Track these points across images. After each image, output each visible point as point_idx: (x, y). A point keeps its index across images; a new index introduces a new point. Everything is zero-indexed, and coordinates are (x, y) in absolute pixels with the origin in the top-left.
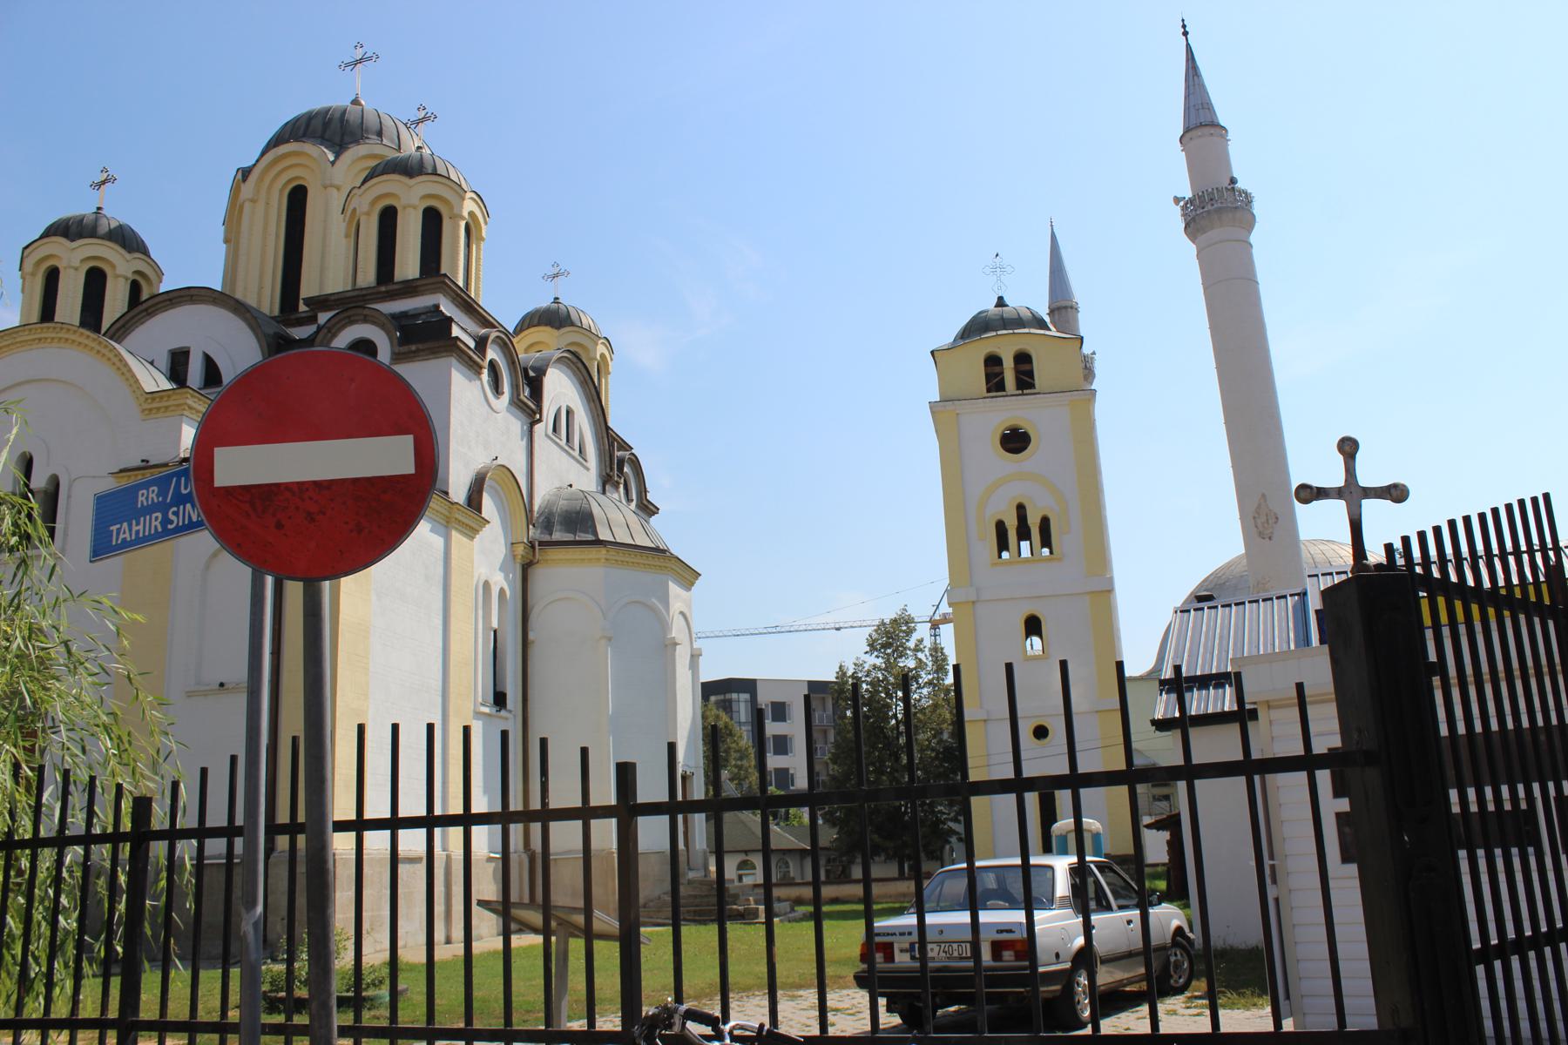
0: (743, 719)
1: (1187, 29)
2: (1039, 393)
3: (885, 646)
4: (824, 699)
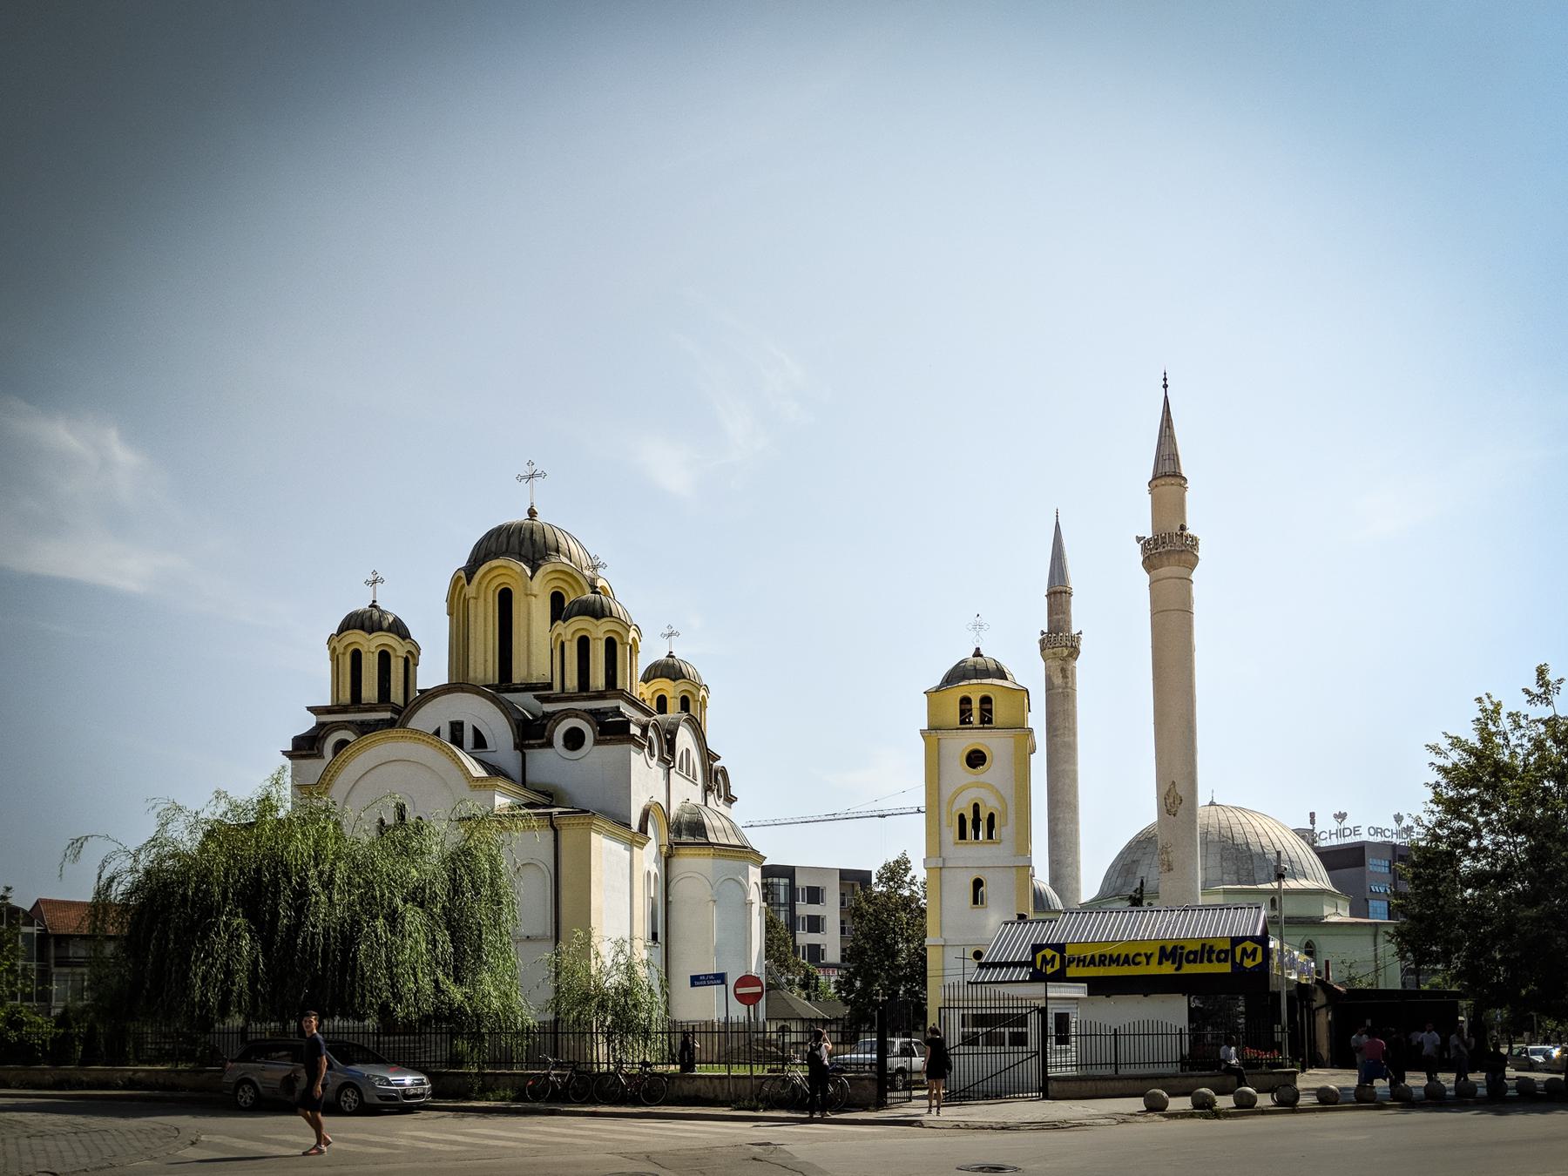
0: (782, 901)
1: (1163, 383)
2: (994, 728)
3: (889, 879)
4: (853, 885)
